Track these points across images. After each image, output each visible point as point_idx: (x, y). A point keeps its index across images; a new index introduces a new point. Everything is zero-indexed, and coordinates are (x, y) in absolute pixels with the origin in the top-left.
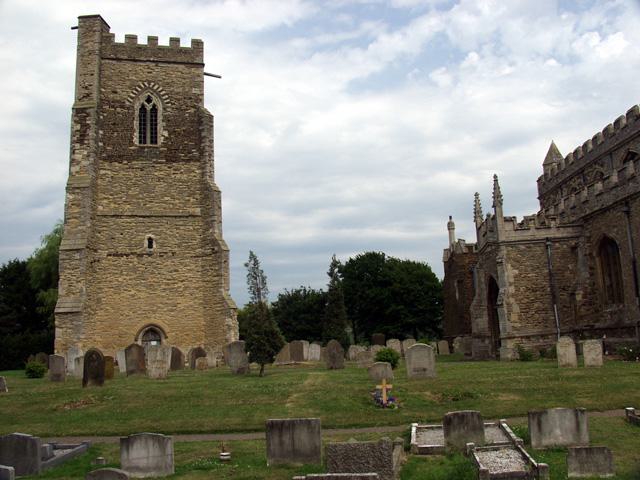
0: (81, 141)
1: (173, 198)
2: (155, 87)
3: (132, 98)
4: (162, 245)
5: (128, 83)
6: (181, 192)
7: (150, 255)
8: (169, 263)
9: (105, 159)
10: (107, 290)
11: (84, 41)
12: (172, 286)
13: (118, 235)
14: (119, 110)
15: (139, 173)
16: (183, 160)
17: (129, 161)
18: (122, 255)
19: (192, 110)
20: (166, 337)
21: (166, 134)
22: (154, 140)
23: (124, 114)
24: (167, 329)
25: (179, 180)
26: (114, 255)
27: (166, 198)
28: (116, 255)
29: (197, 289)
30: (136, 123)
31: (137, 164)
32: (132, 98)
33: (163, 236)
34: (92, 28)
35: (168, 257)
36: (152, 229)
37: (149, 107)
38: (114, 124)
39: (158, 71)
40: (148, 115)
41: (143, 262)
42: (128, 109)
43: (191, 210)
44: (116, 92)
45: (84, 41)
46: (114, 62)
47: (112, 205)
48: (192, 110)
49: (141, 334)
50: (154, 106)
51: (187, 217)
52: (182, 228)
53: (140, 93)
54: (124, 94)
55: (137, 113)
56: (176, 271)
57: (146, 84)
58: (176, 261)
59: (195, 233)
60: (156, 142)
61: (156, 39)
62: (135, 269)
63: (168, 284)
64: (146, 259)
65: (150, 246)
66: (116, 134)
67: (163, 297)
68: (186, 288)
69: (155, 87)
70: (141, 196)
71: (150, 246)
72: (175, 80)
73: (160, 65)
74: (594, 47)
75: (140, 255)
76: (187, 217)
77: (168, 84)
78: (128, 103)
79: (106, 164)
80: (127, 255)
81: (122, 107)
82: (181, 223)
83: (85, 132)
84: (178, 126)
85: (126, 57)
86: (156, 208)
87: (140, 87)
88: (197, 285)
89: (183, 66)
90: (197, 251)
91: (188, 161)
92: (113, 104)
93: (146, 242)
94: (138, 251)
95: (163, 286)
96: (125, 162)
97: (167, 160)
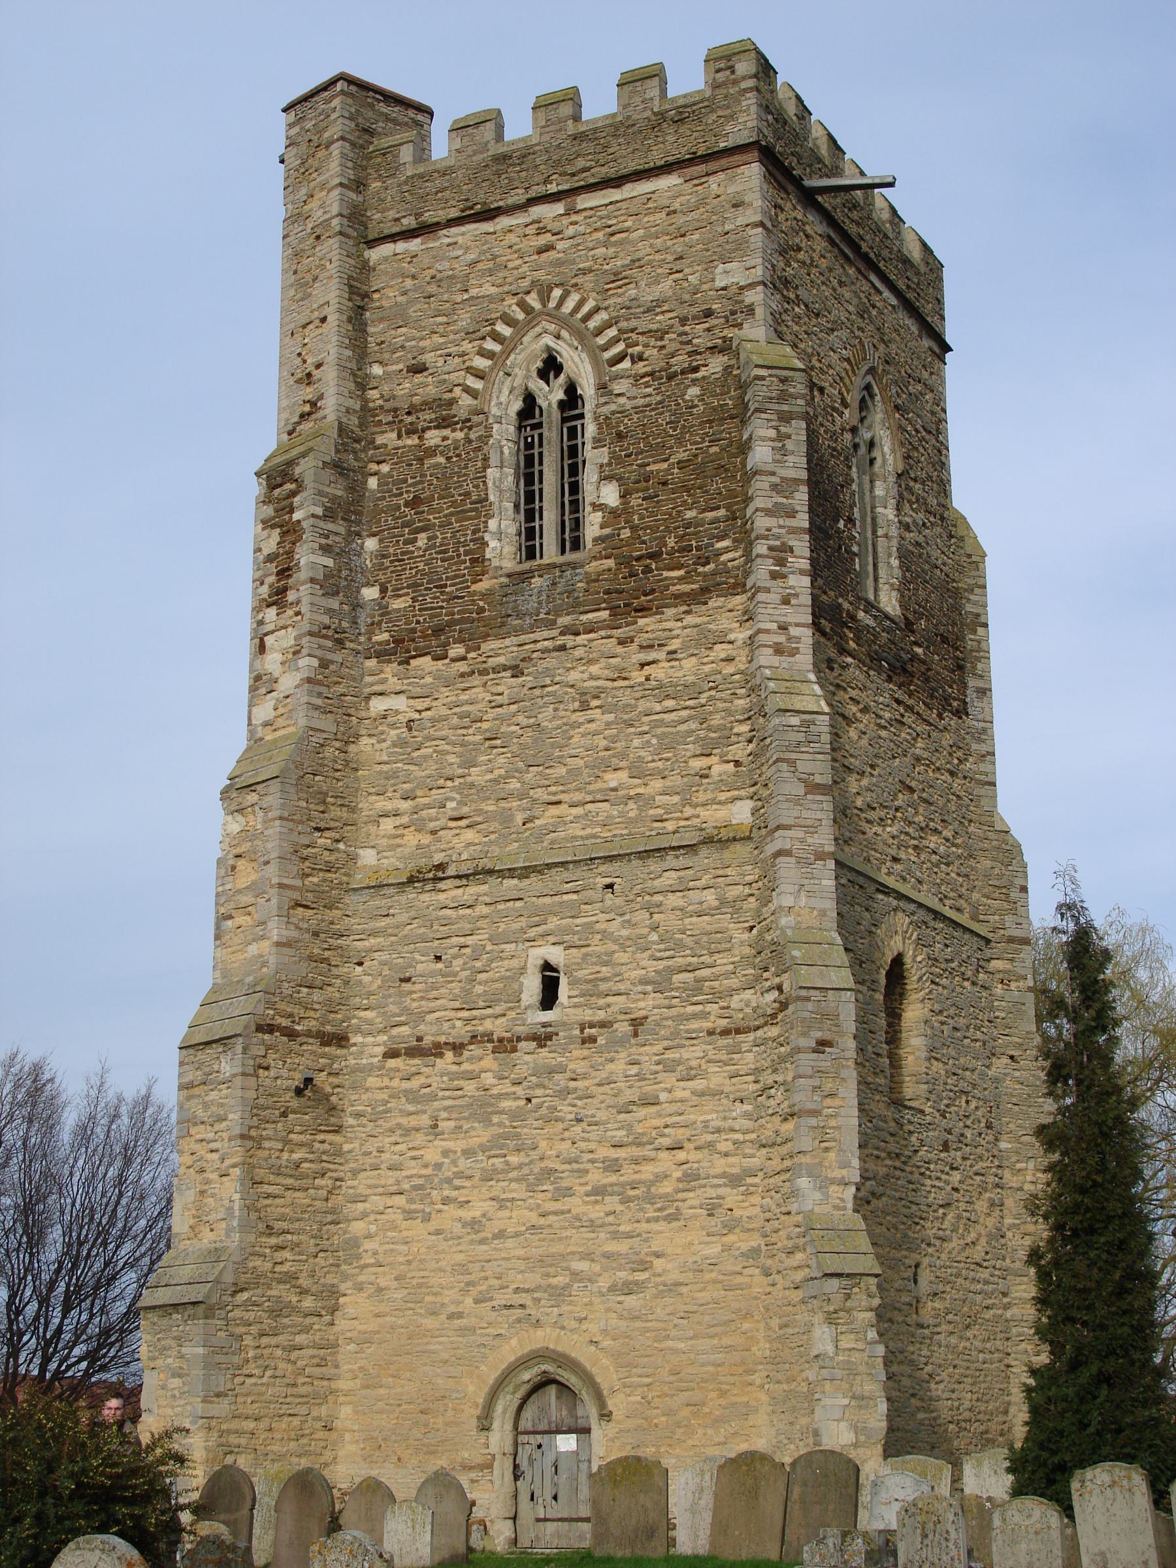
0: (278, 598)
1: (639, 772)
2: (569, 305)
3: (480, 375)
4: (591, 990)
5: (464, 319)
6: (668, 744)
7: (542, 1039)
8: (619, 1067)
9: (382, 654)
10: (378, 1202)
11: (602, 400)
12: (628, 1174)
13: (424, 965)
14: (433, 437)
15: (507, 685)
16: (679, 598)
17: (472, 642)
18: (437, 1050)
19: (715, 365)
20: (606, 1416)
21: (610, 495)
22: (572, 540)
23: (452, 452)
24: (606, 1374)
25: (663, 691)
26: (412, 1052)
27: (613, 779)
28: (417, 1051)
29: (734, 1181)
30: (501, 481)
31: (500, 649)
32: (480, 375)
33: (597, 947)
34: (356, 126)
35: (618, 1043)
36: (553, 923)
37: (551, 395)
38: (415, 502)
39: (576, 231)
40: (552, 433)
41: (521, 1071)
42: (467, 424)
43: (712, 816)
44: (418, 369)
45: (602, 400)
46: (415, 245)
47: (411, 839)
48: (715, 365)
49: (507, 1403)
50: (571, 389)
51: (691, 848)
52: (674, 900)
53: (509, 345)
54: (451, 366)
55: (504, 435)
56: (650, 1101)
57: (533, 300)
58: (648, 1054)
59: (724, 920)
60: (576, 545)
61: (572, 97)
62: (483, 1108)
63: (613, 1166)
64: (527, 1057)
65: (549, 998)
66: (422, 540)
67: (593, 1226)
68: (691, 1179)
69: (569, 305)
70: (514, 785)
71: (549, 998)
72: (644, 249)
73: (585, 201)
74: (758, 556)
75: (505, 1046)
76: (691, 848)
77: (617, 276)
78: (466, 401)
79: (390, 669)
80: (457, 1048)
81: (444, 423)
82: (670, 878)
83: (290, 554)
84: (659, 451)
85: (454, 213)
86: (574, 826)
87: (509, 321)
88: (734, 1164)
89: (670, 181)
90: (735, 1002)
91: (699, 597)
92: (407, 419)
93: (532, 986)
94: (498, 1028)
95: (596, 1177)
96: (456, 650)
97: (614, 610)
